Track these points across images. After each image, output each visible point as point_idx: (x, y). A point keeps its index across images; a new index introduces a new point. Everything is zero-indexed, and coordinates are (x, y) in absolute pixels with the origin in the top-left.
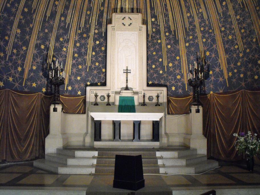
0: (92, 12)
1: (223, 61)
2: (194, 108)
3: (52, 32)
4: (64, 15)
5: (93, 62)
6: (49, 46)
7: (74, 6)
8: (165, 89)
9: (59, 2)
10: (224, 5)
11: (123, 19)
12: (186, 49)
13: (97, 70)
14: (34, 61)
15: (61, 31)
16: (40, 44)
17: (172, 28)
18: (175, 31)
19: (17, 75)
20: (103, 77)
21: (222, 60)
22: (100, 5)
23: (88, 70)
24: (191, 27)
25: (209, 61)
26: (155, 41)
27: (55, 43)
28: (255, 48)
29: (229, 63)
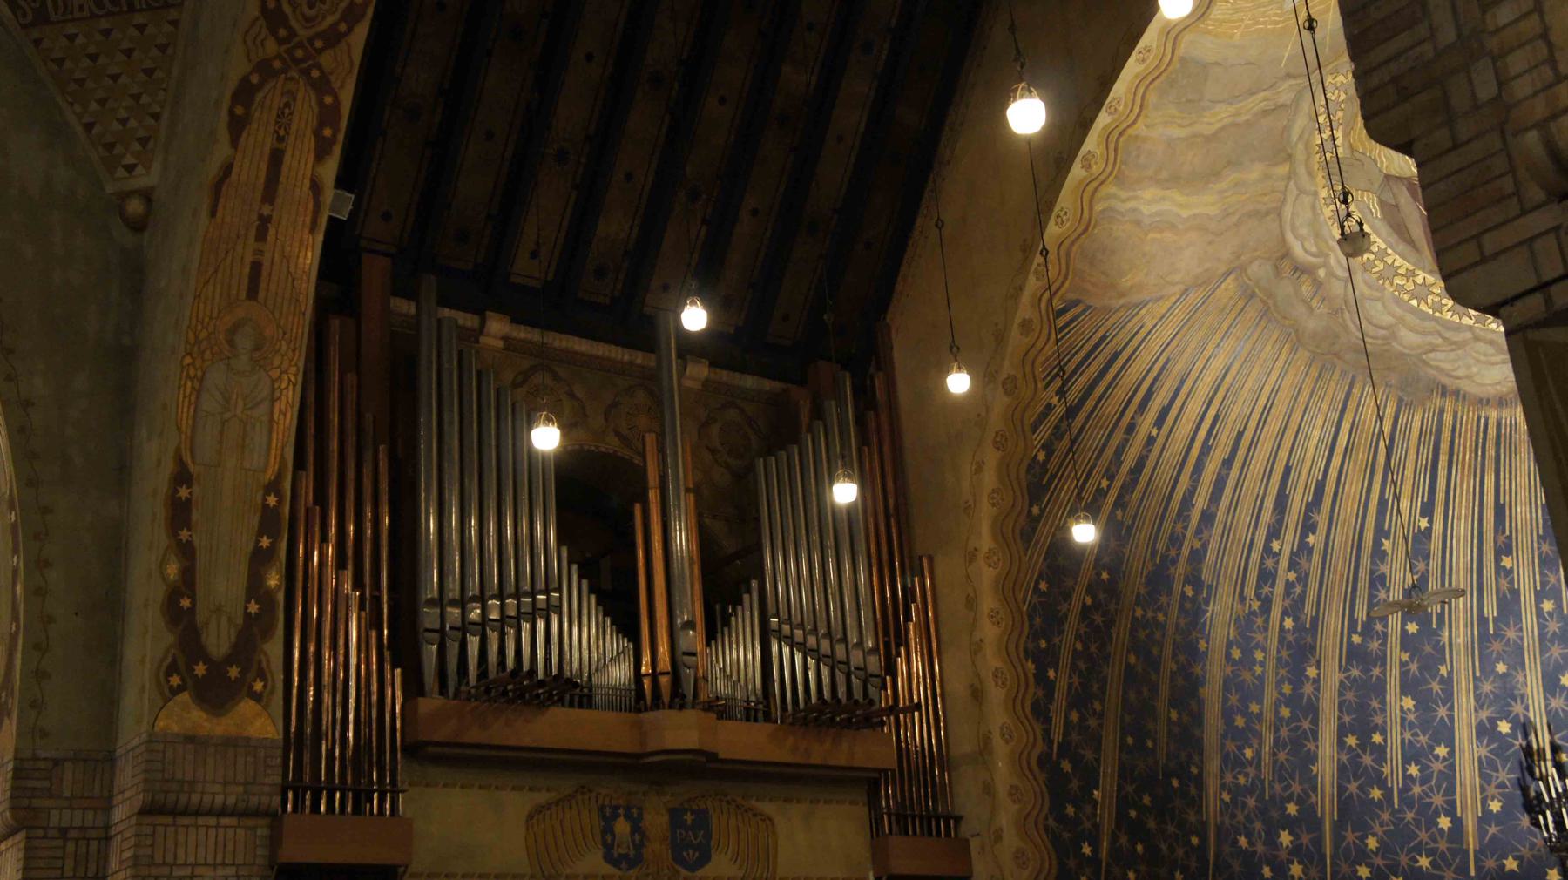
6: (1526, 717)
16: (1493, 722)
27: (1546, 698)
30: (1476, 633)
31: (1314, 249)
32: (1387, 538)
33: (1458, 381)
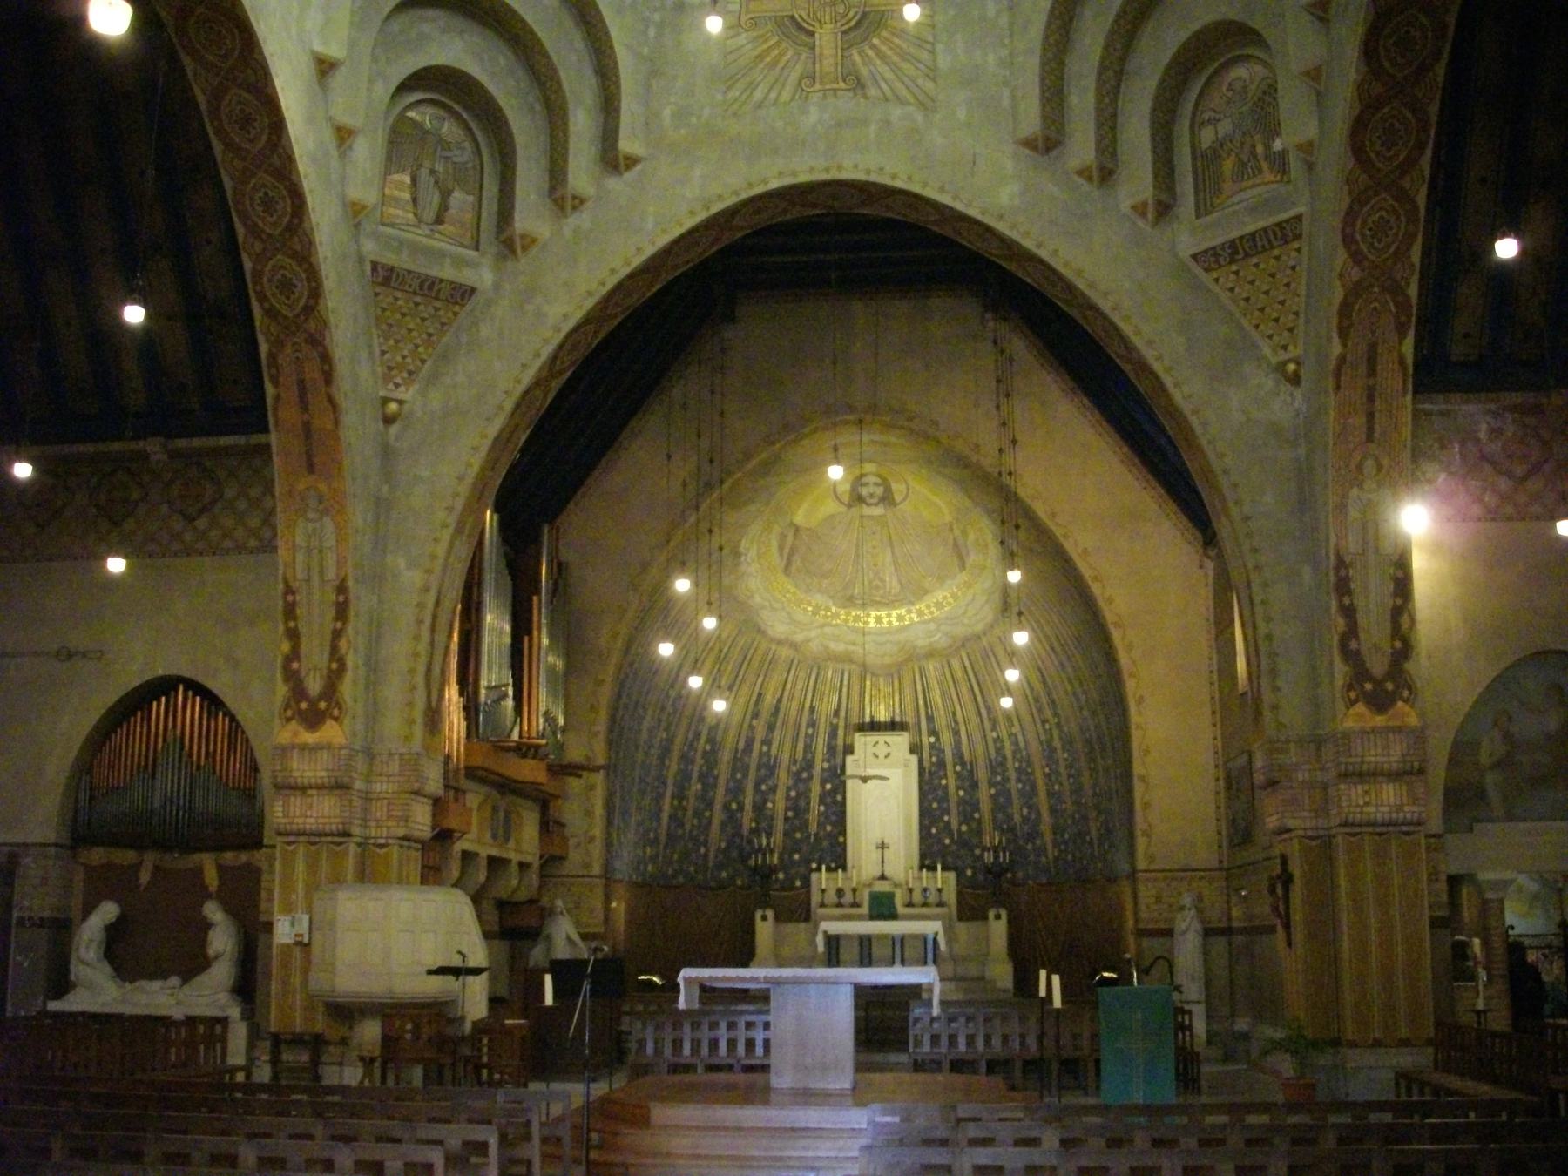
2: (991, 914)
5: (821, 825)
15: (763, 771)
19: (700, 862)
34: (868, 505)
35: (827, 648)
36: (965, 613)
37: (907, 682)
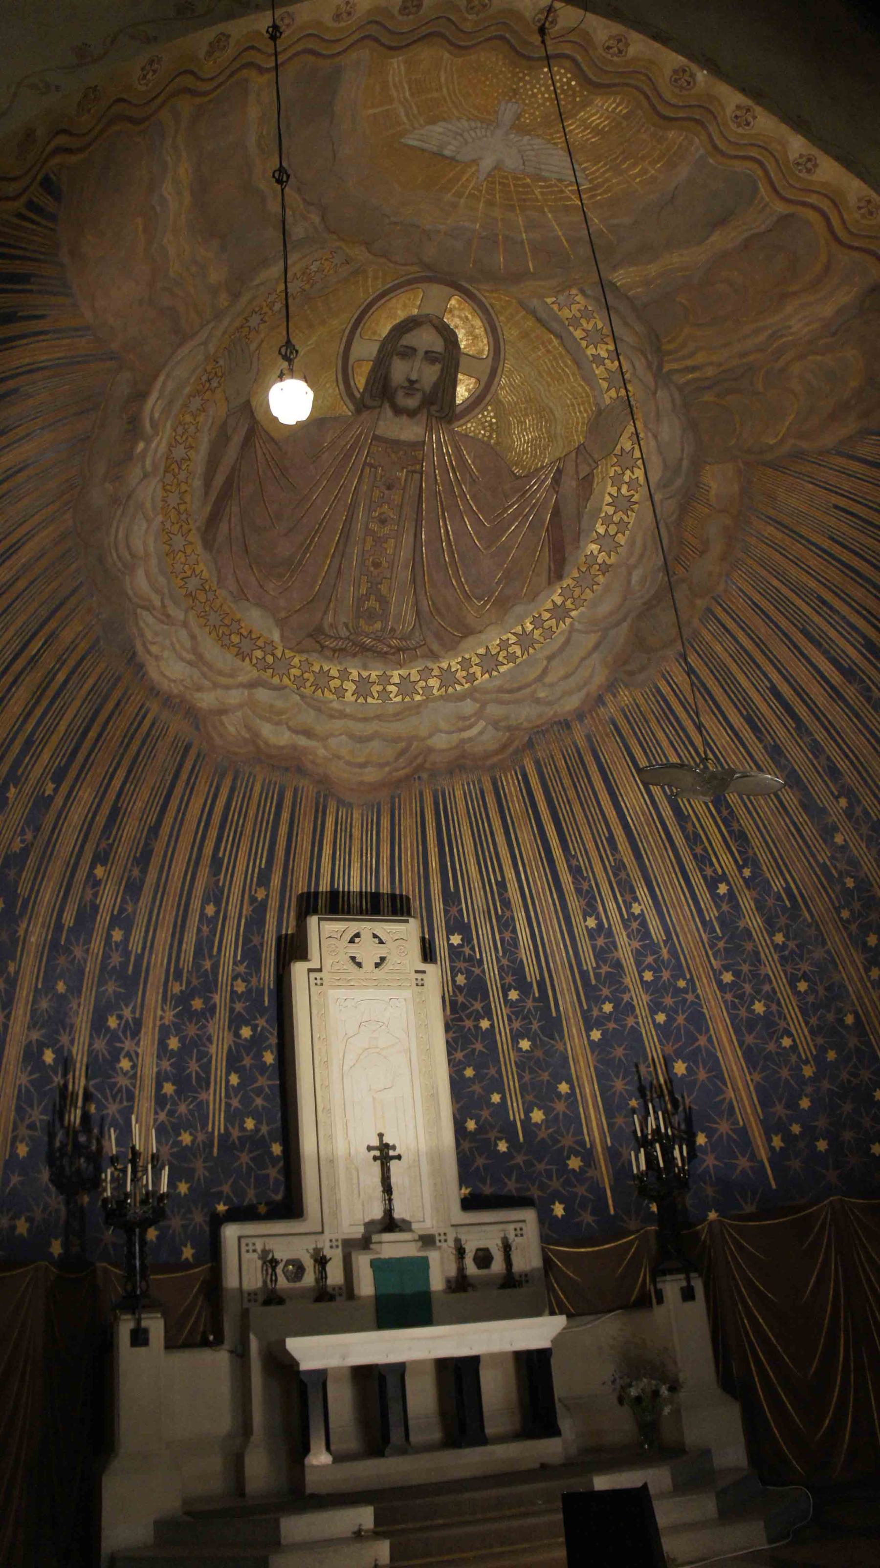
0: (223, 905)
1: (743, 1093)
2: (671, 1287)
3: (80, 992)
4: (122, 920)
5: (233, 1117)
6: (70, 1051)
7: (158, 885)
8: (529, 1216)
9: (108, 868)
10: (724, 894)
11: (352, 941)
12: (593, 1052)
13: (251, 1151)
14: (22, 1120)
15: (111, 988)
16: (41, 1046)
17: (531, 973)
18: (541, 984)
20: (276, 1180)
21: (739, 1090)
22: (255, 880)
23: (215, 1150)
24: (605, 969)
25: (688, 1097)
26: (469, 1024)
27: (91, 1036)
28: (855, 1045)
29: (765, 1100)
30: (49, 937)
31: (156, 415)
32: (15, 787)
33: (148, 657)
34: (398, 411)
35: (256, 735)
36: (540, 678)
37: (408, 824)
